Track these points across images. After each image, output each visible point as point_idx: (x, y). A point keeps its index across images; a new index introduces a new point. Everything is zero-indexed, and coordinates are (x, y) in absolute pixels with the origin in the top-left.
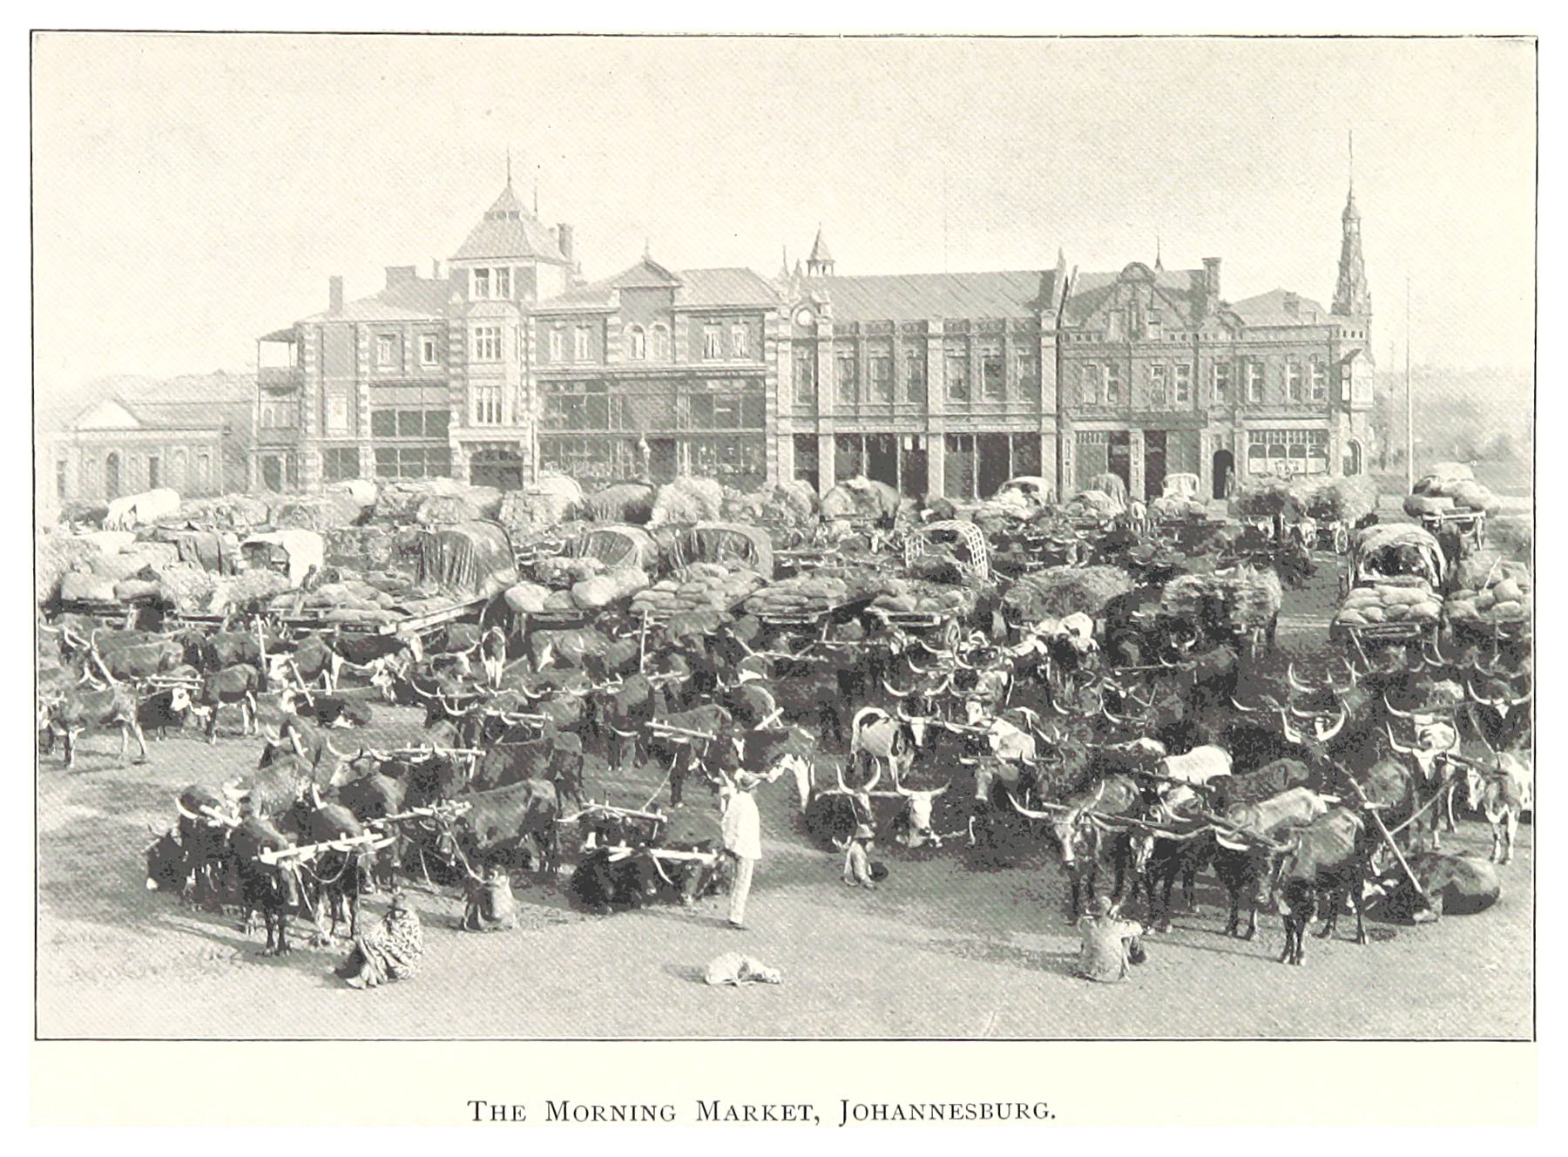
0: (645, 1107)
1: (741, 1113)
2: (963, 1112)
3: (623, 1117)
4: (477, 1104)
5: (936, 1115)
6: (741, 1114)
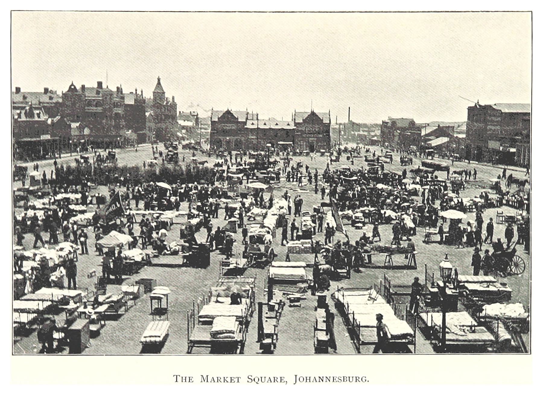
0: (327, 377)
1: (216, 380)
2: (337, 379)
3: (323, 381)
4: (177, 376)
5: (327, 380)
6: (216, 380)
